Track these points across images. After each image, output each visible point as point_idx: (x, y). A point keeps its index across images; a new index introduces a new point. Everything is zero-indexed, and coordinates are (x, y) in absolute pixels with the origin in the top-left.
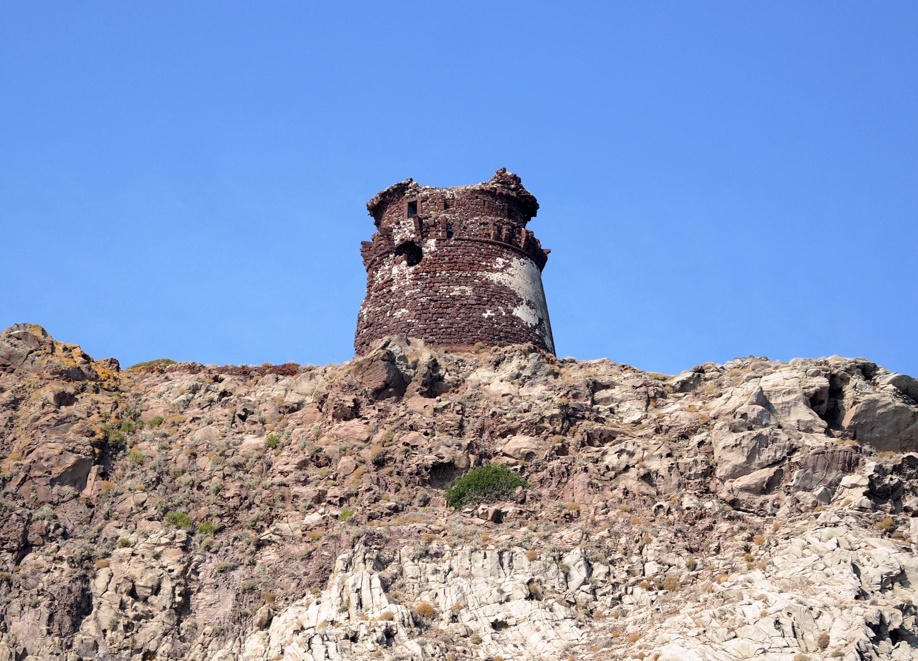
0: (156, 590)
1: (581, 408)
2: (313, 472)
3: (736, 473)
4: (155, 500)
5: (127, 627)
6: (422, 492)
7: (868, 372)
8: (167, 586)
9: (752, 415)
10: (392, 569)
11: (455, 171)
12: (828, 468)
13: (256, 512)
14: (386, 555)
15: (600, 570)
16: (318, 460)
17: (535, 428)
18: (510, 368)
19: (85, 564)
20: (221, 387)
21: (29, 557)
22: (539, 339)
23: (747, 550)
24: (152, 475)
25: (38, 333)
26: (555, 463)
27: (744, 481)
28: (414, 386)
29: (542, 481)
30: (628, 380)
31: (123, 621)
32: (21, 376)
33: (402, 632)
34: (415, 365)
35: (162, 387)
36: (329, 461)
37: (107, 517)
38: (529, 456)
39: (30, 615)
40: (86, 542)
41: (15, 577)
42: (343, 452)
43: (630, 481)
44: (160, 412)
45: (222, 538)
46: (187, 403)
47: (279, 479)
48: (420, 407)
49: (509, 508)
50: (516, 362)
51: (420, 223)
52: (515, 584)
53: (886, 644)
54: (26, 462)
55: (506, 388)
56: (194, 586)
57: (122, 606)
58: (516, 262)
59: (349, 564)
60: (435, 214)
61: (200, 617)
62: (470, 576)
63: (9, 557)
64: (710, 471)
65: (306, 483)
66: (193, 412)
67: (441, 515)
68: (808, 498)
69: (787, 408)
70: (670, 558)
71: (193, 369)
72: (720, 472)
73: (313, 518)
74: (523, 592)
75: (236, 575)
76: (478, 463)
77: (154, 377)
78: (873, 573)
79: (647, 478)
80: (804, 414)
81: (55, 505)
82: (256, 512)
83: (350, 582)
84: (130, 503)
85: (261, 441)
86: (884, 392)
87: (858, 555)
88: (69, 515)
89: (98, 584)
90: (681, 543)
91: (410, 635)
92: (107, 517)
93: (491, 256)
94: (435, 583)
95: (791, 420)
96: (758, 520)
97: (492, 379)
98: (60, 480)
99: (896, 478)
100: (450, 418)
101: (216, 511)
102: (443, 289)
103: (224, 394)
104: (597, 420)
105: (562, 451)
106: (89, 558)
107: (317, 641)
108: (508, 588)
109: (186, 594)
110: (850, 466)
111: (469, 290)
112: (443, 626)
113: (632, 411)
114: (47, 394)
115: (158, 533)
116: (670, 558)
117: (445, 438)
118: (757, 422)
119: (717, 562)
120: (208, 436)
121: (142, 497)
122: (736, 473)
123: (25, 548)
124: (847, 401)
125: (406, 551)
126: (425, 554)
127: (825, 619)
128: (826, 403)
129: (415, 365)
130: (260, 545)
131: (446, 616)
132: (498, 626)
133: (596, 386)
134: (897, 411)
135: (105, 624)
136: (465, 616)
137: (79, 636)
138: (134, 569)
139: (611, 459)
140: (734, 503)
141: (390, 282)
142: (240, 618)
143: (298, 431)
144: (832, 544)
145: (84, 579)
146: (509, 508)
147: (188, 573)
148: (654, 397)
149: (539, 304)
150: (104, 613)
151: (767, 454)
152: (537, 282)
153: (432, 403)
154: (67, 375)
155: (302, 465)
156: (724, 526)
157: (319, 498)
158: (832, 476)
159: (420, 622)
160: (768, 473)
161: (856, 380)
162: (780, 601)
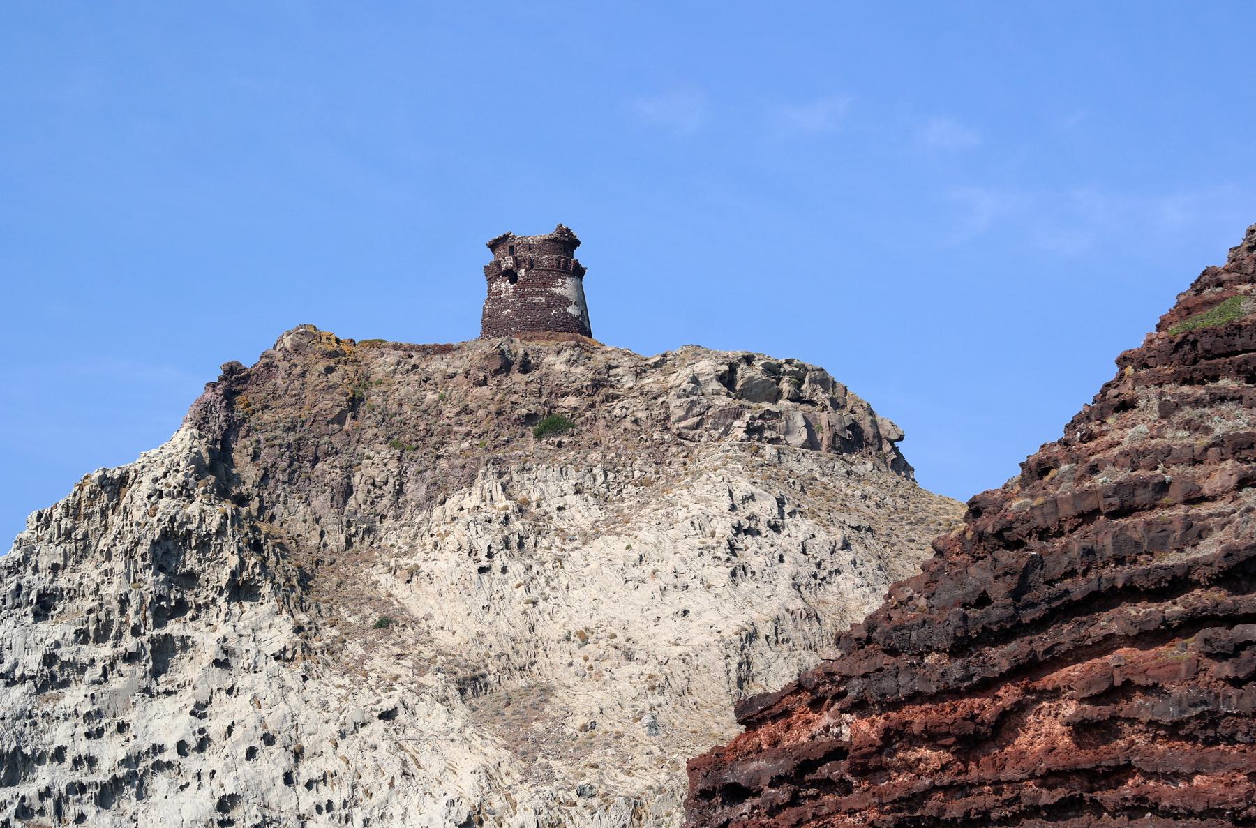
0: (386, 483)
1: (603, 380)
2: (464, 418)
3: (680, 419)
4: (382, 434)
5: (372, 503)
6: (521, 430)
7: (749, 360)
8: (391, 481)
9: (689, 390)
10: (507, 477)
11: (538, 228)
12: (726, 418)
13: (435, 439)
14: (504, 470)
15: (611, 476)
16: (466, 411)
17: (578, 393)
18: (565, 355)
19: (349, 469)
20: (413, 361)
21: (319, 465)
22: (581, 327)
23: (685, 464)
24: (380, 417)
25: (312, 330)
26: (588, 414)
27: (684, 423)
28: (515, 367)
29: (582, 423)
30: (626, 362)
31: (369, 500)
32: (306, 357)
33: (513, 517)
34: (516, 354)
35: (380, 360)
36: (472, 412)
37: (358, 442)
38: (575, 409)
39: (321, 498)
40: (346, 457)
41: (313, 476)
42: (480, 407)
43: (627, 423)
44: (380, 376)
45: (418, 453)
46: (395, 371)
47: (446, 421)
48: (518, 380)
49: (566, 439)
50: (568, 352)
51: (515, 259)
52: (568, 485)
53: (741, 536)
54: (314, 412)
55: (563, 368)
56: (405, 480)
57: (369, 491)
58: (568, 280)
59: (485, 474)
60: (524, 254)
61: (409, 497)
62: (546, 481)
63: (308, 465)
64: (668, 418)
65: (461, 424)
66: (398, 377)
67: (531, 445)
68: (716, 434)
69: (707, 382)
70: (646, 468)
71: (396, 347)
72: (672, 419)
73: (465, 445)
74: (572, 491)
75: (426, 474)
76: (550, 412)
77: (375, 352)
78: (738, 495)
79: (636, 422)
80: (716, 385)
81: (330, 435)
82: (435, 439)
83: (486, 487)
84: (369, 435)
85: (436, 397)
86: (756, 372)
87: (732, 485)
88: (338, 441)
89: (356, 480)
90: (652, 460)
91: (518, 519)
92: (358, 442)
93: (554, 278)
94: (528, 485)
95: (709, 389)
96: (691, 444)
97: (557, 361)
98: (332, 421)
99: (760, 422)
100: (534, 387)
101: (414, 438)
102: (529, 299)
103: (415, 366)
104: (612, 386)
105: (593, 406)
106: (350, 466)
107: (471, 524)
108: (565, 489)
109: (401, 485)
110: (738, 415)
111: (543, 299)
112: (533, 510)
113: (629, 382)
114: (321, 367)
115: (385, 452)
116: (646, 468)
117: (532, 398)
118: (692, 393)
119: (670, 470)
120: (408, 393)
121: (375, 430)
122: (680, 419)
123: (316, 460)
124: (738, 376)
125: (514, 468)
126: (524, 469)
127: (714, 522)
128: (728, 380)
129: (516, 354)
130: (438, 457)
131: (534, 504)
132: (560, 509)
133: (610, 367)
134: (764, 381)
135: (360, 501)
136: (544, 504)
137: (347, 508)
138: (374, 472)
139: (617, 411)
140: (680, 435)
141: (500, 292)
142: (430, 498)
143: (456, 390)
144: (720, 479)
145: (348, 477)
146: (566, 439)
147: (401, 475)
148: (639, 374)
149: (582, 302)
150: (359, 495)
151: (696, 410)
152: (580, 288)
153: (525, 377)
154: (330, 355)
155: (458, 414)
156: (673, 449)
157: (468, 434)
158: (728, 422)
159: (521, 510)
160: (696, 420)
161: (743, 365)
162: (695, 510)
